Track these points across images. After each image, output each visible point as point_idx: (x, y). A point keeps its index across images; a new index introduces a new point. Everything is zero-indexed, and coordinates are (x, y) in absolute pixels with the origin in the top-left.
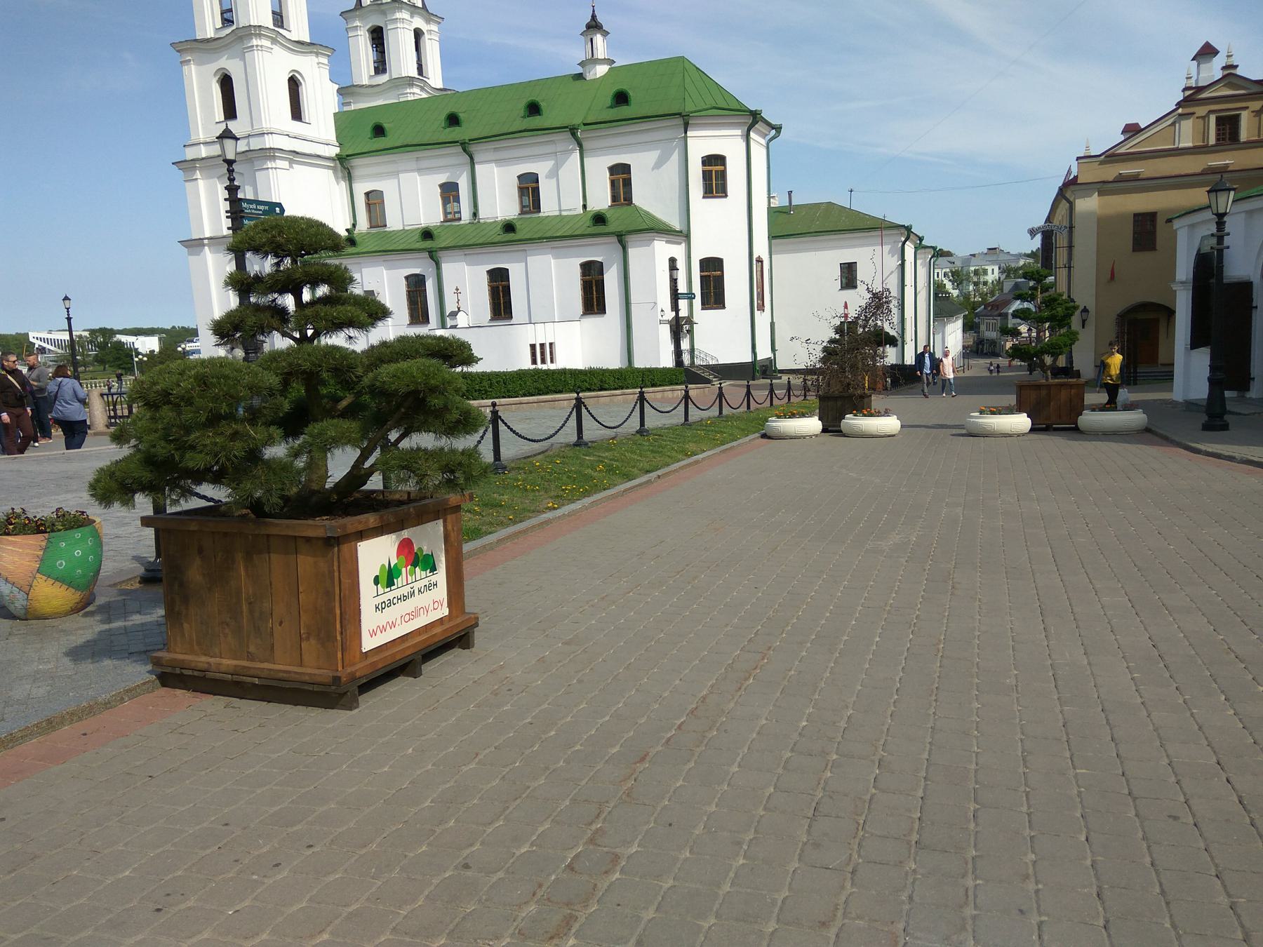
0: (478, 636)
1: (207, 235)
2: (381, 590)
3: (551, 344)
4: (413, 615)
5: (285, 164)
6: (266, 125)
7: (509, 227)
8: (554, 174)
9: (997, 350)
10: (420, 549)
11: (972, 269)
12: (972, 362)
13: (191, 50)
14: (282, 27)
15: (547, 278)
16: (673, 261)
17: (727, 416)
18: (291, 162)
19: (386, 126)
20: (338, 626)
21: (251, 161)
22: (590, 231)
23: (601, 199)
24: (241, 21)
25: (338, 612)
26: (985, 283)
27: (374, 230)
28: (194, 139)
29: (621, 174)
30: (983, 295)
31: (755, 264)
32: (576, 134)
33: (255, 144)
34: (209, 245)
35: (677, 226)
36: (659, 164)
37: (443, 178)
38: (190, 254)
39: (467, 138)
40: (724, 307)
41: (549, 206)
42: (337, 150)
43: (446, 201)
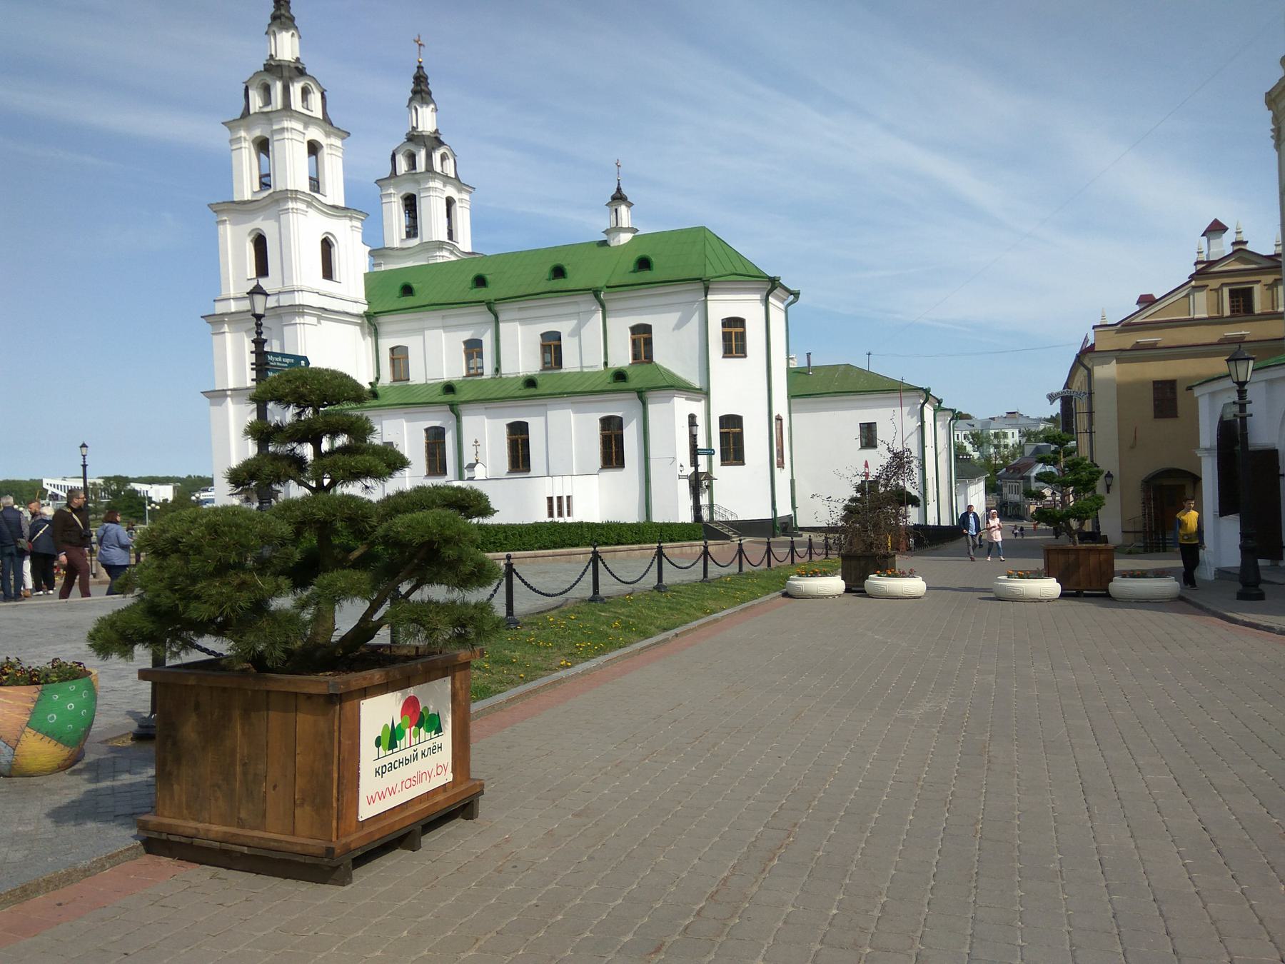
0: (483, 805)
1: (231, 386)
2: (382, 753)
3: (568, 497)
4: (414, 781)
5: (314, 320)
6: (297, 283)
7: (530, 382)
8: (576, 332)
9: (1021, 513)
10: (426, 709)
14: (318, 192)
15: (567, 432)
18: (320, 318)
23: (622, 356)
24: (279, 185)
25: (335, 775)
26: (1006, 446)
29: (642, 336)
31: (774, 421)
33: (285, 300)
34: (231, 396)
35: (696, 382)
36: (679, 326)
37: (468, 335)
38: (212, 404)
39: (492, 298)
40: (743, 464)
41: (570, 362)
42: (366, 308)
43: (469, 356)
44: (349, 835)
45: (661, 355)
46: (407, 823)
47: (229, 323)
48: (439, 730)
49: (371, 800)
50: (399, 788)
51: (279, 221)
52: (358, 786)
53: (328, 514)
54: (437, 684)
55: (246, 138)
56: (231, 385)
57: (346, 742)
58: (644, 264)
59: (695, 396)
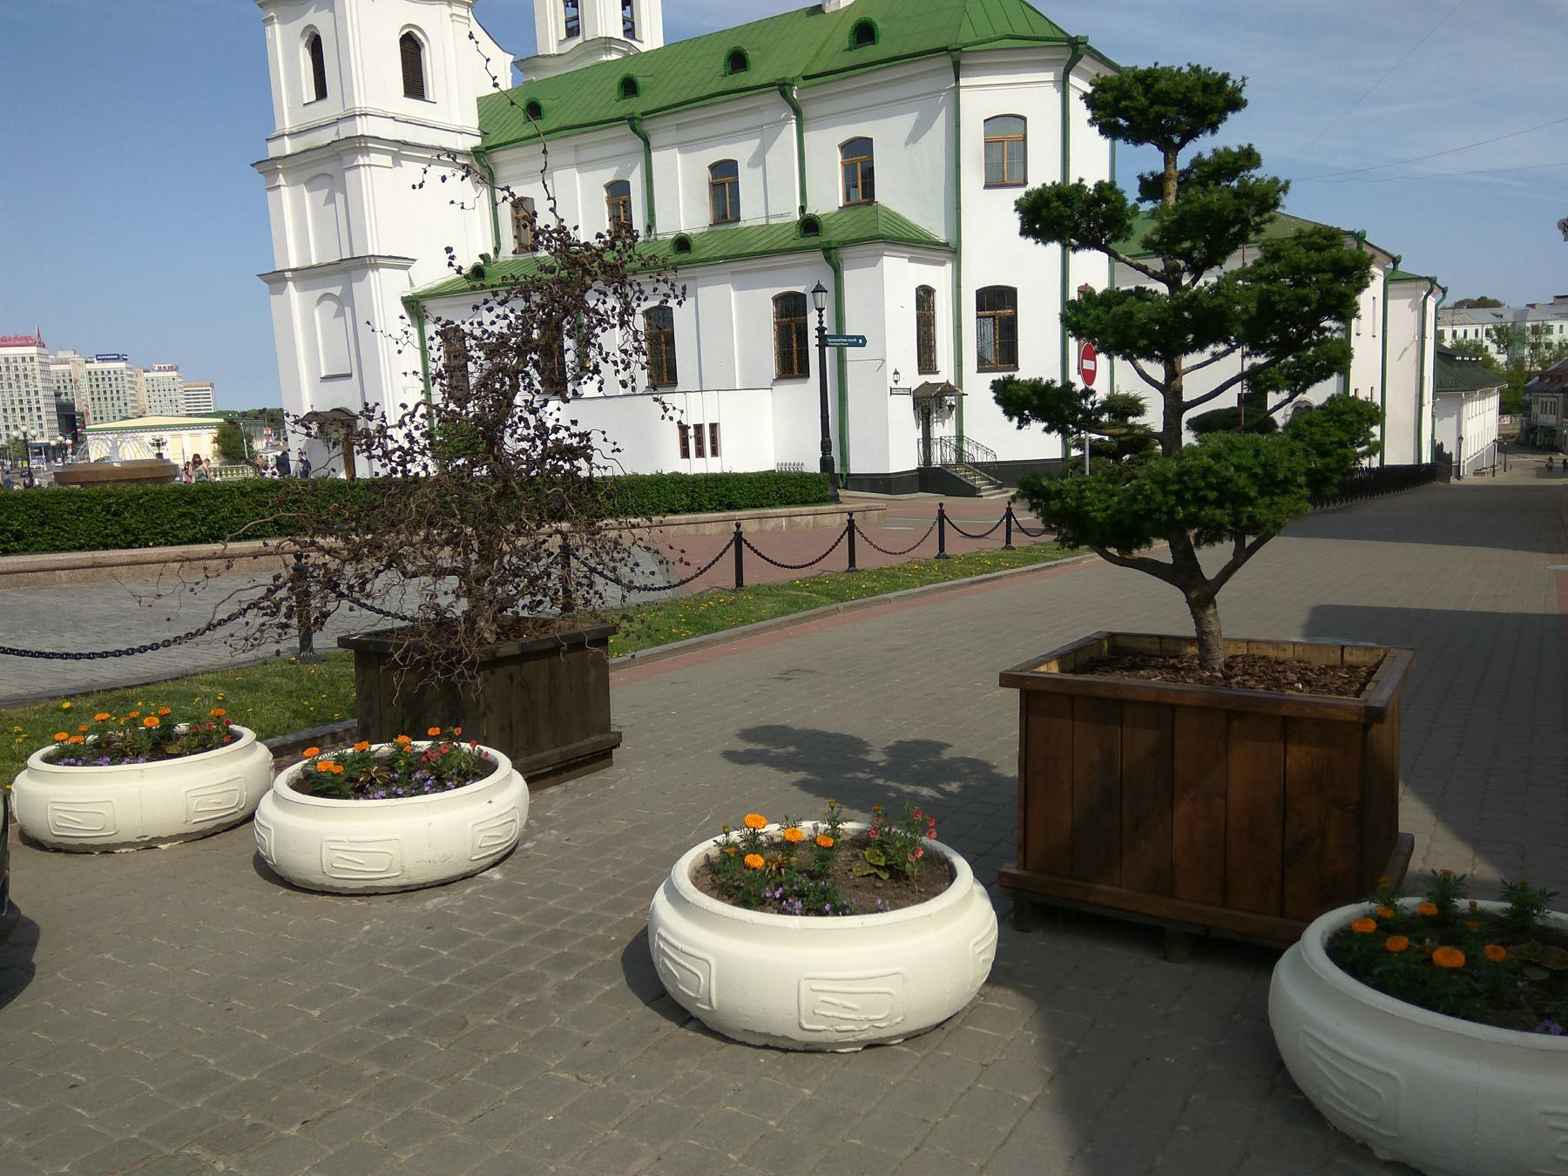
1: (294, 265)
5: (387, 160)
6: (360, 103)
8: (759, 160)
9: (1557, 442)
11: (1529, 325)
12: (1513, 459)
14: (633, 38)
15: (727, 321)
16: (925, 296)
17: (757, 591)
18: (397, 159)
19: (543, 103)
21: (338, 157)
22: (794, 244)
23: (828, 196)
26: (1549, 346)
27: (522, 257)
28: (278, 130)
29: (858, 156)
30: (1542, 362)
32: (793, 95)
33: (345, 130)
35: (942, 237)
36: (915, 136)
37: (609, 175)
38: (272, 293)
39: (638, 111)
41: (751, 212)
42: (477, 141)
43: (613, 205)
45: (886, 193)
47: (285, 171)
51: (332, 10)
56: (294, 264)
58: (865, 33)
59: (940, 256)
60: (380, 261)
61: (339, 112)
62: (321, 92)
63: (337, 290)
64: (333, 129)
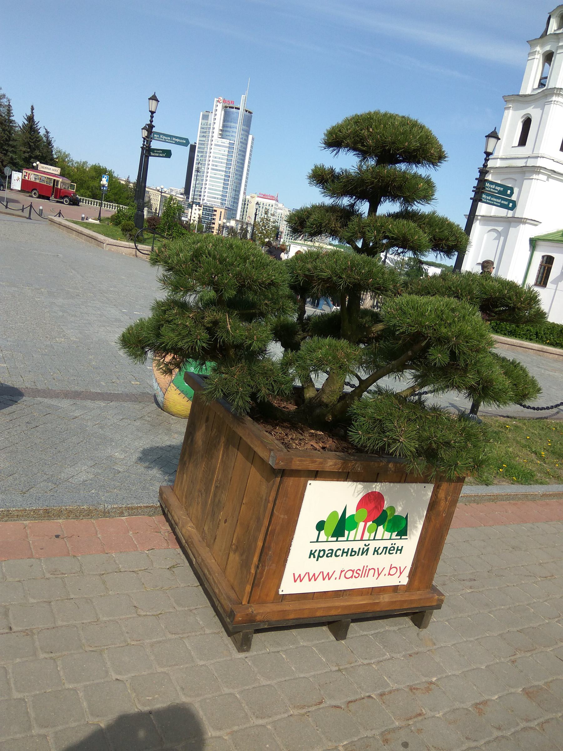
0: (436, 618)
2: (323, 537)
4: (356, 573)
5: (544, 178)
6: (542, 152)
10: (392, 509)
13: (514, 101)
18: (549, 177)
20: (256, 559)
21: (524, 173)
24: (551, 84)
25: (260, 544)
33: (531, 163)
34: (480, 220)
44: (262, 602)
46: (333, 613)
48: (403, 533)
49: (298, 578)
50: (337, 575)
52: (286, 561)
53: (334, 272)
54: (413, 488)
55: (540, 51)
57: (280, 516)
60: (528, 221)
61: (529, 153)
62: (523, 141)
63: (500, 229)
64: (525, 160)
